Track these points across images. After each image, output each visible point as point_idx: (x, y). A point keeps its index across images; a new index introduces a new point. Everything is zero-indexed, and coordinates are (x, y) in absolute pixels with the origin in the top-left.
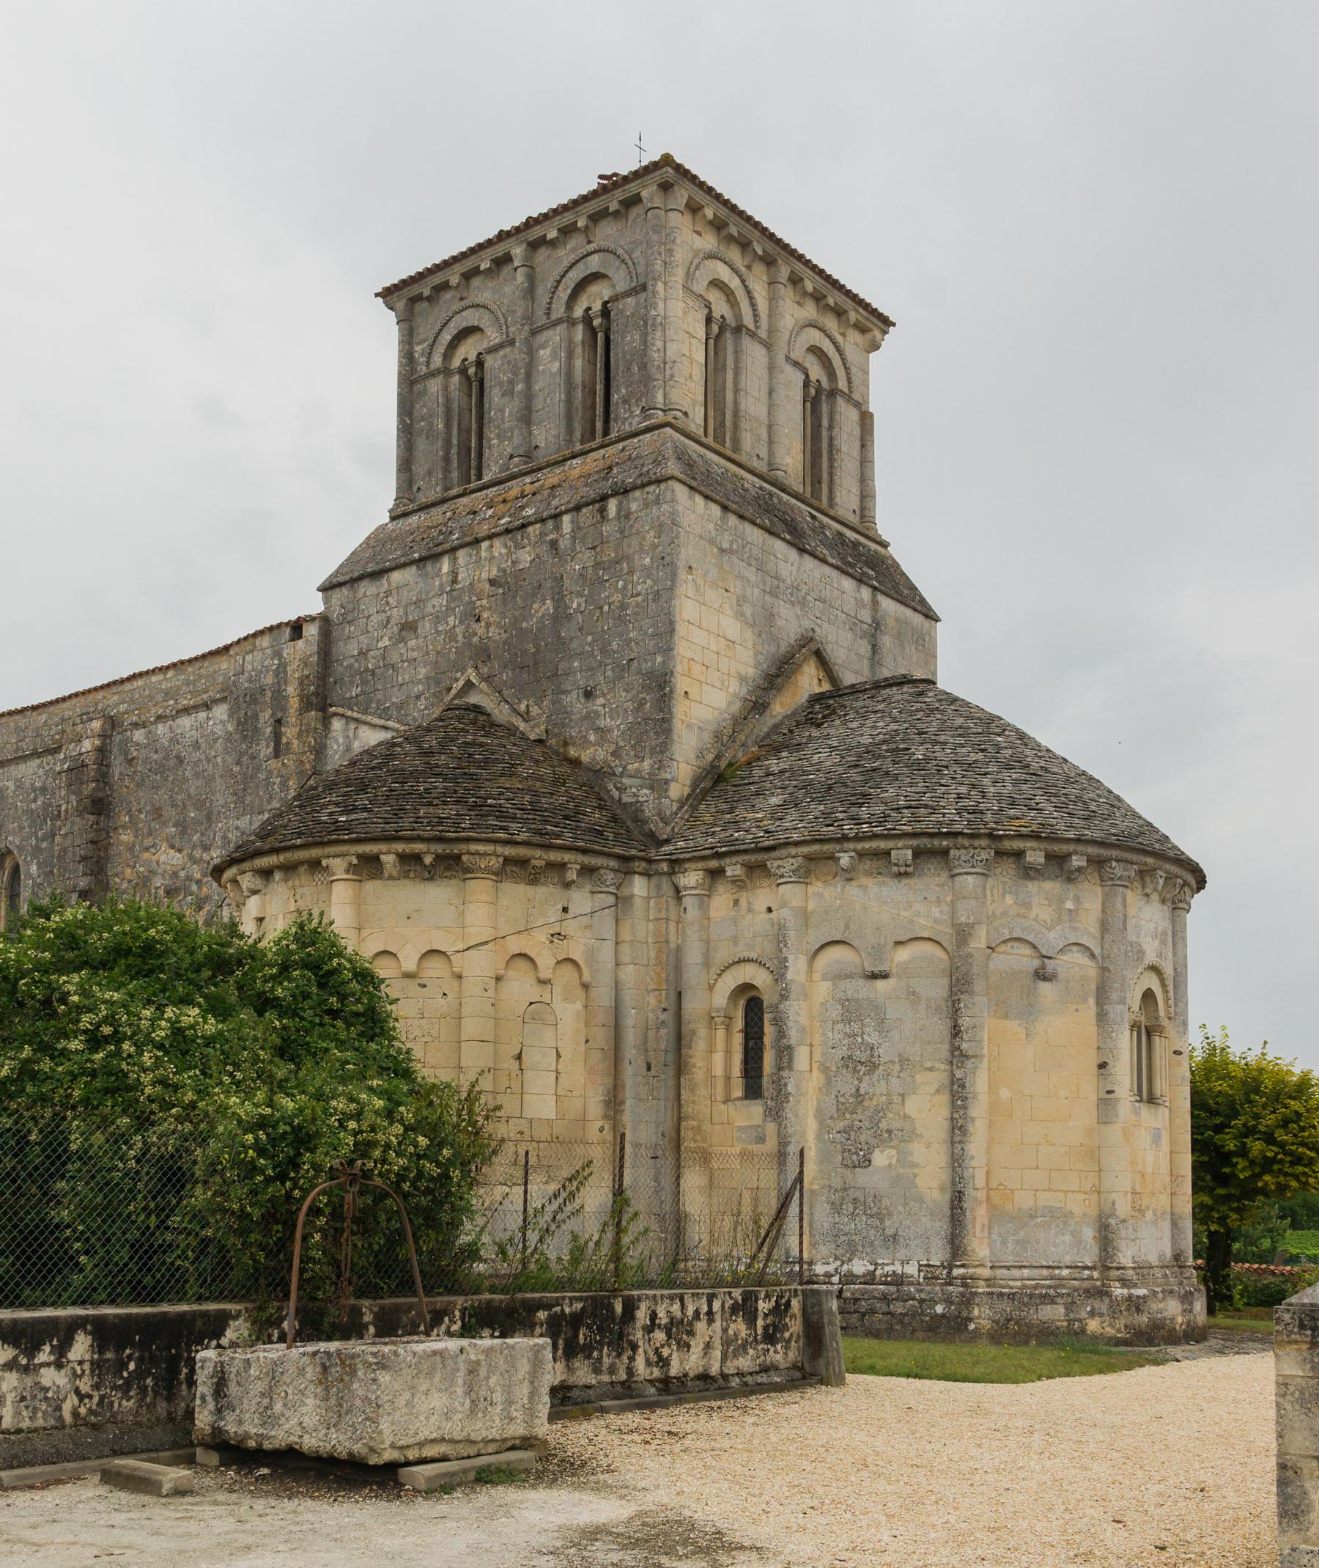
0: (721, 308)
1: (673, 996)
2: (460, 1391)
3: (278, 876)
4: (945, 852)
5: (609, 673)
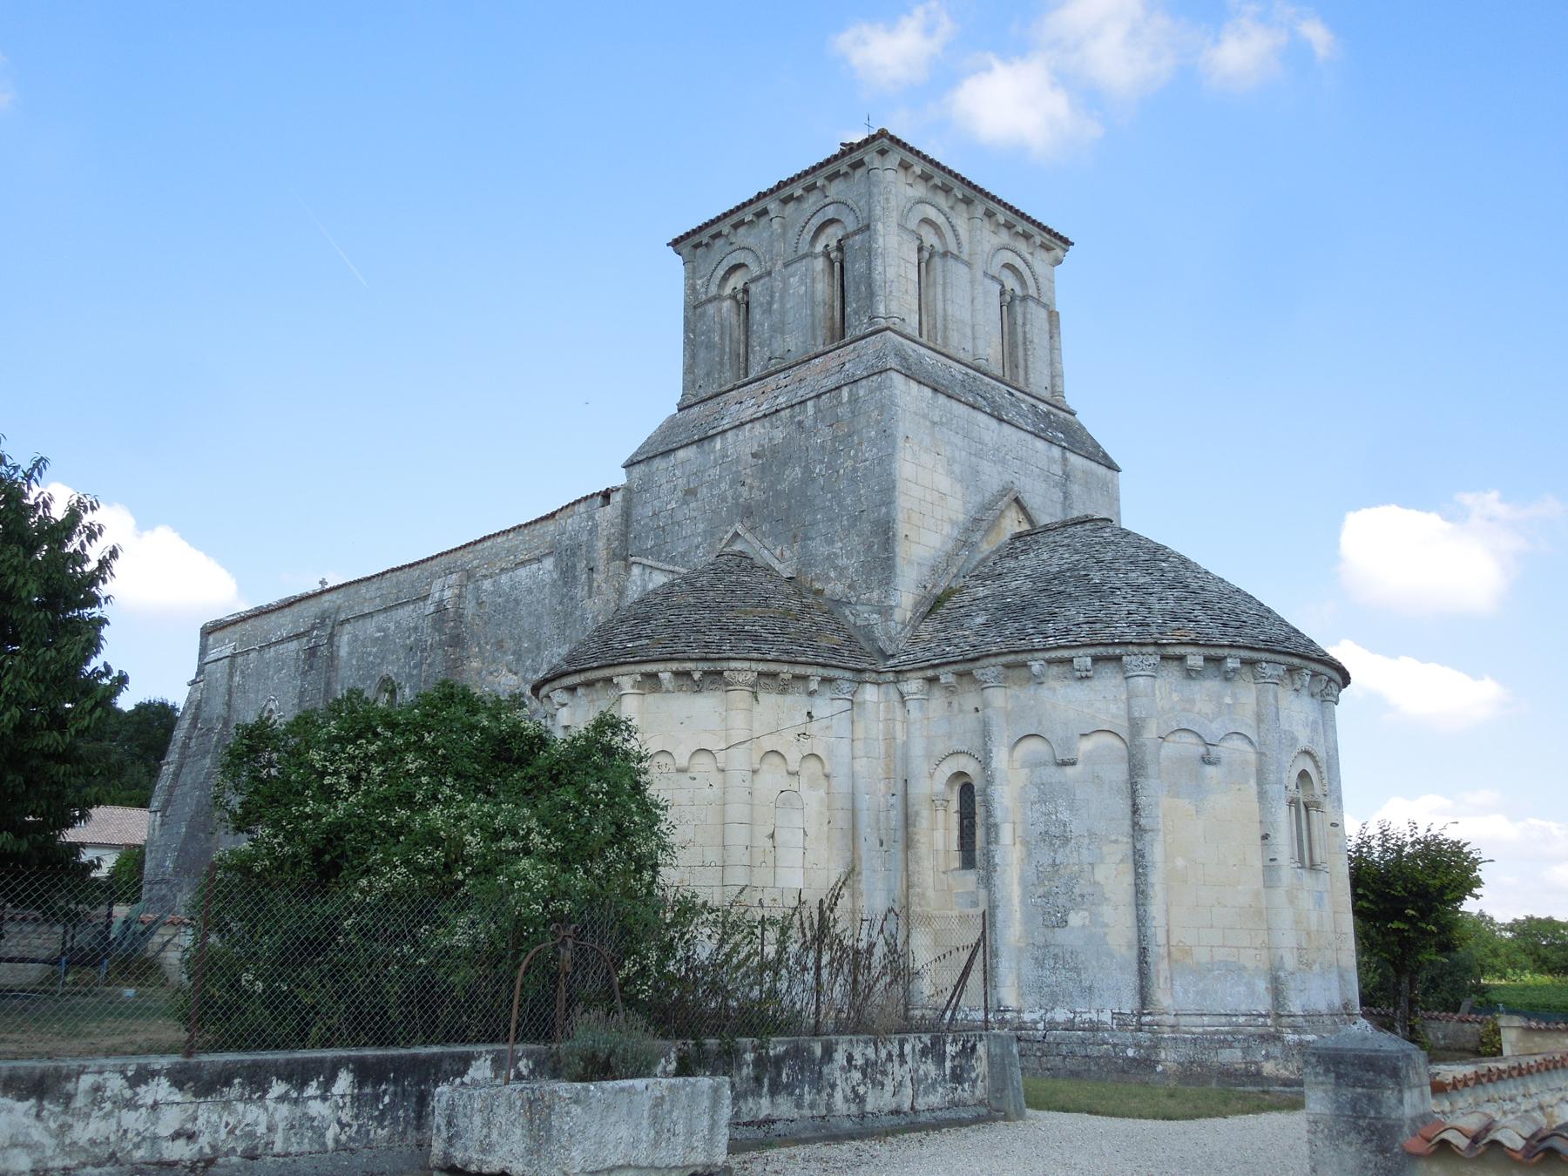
0: (930, 238)
1: (900, 784)
2: (645, 1123)
3: (580, 691)
4: (1119, 658)
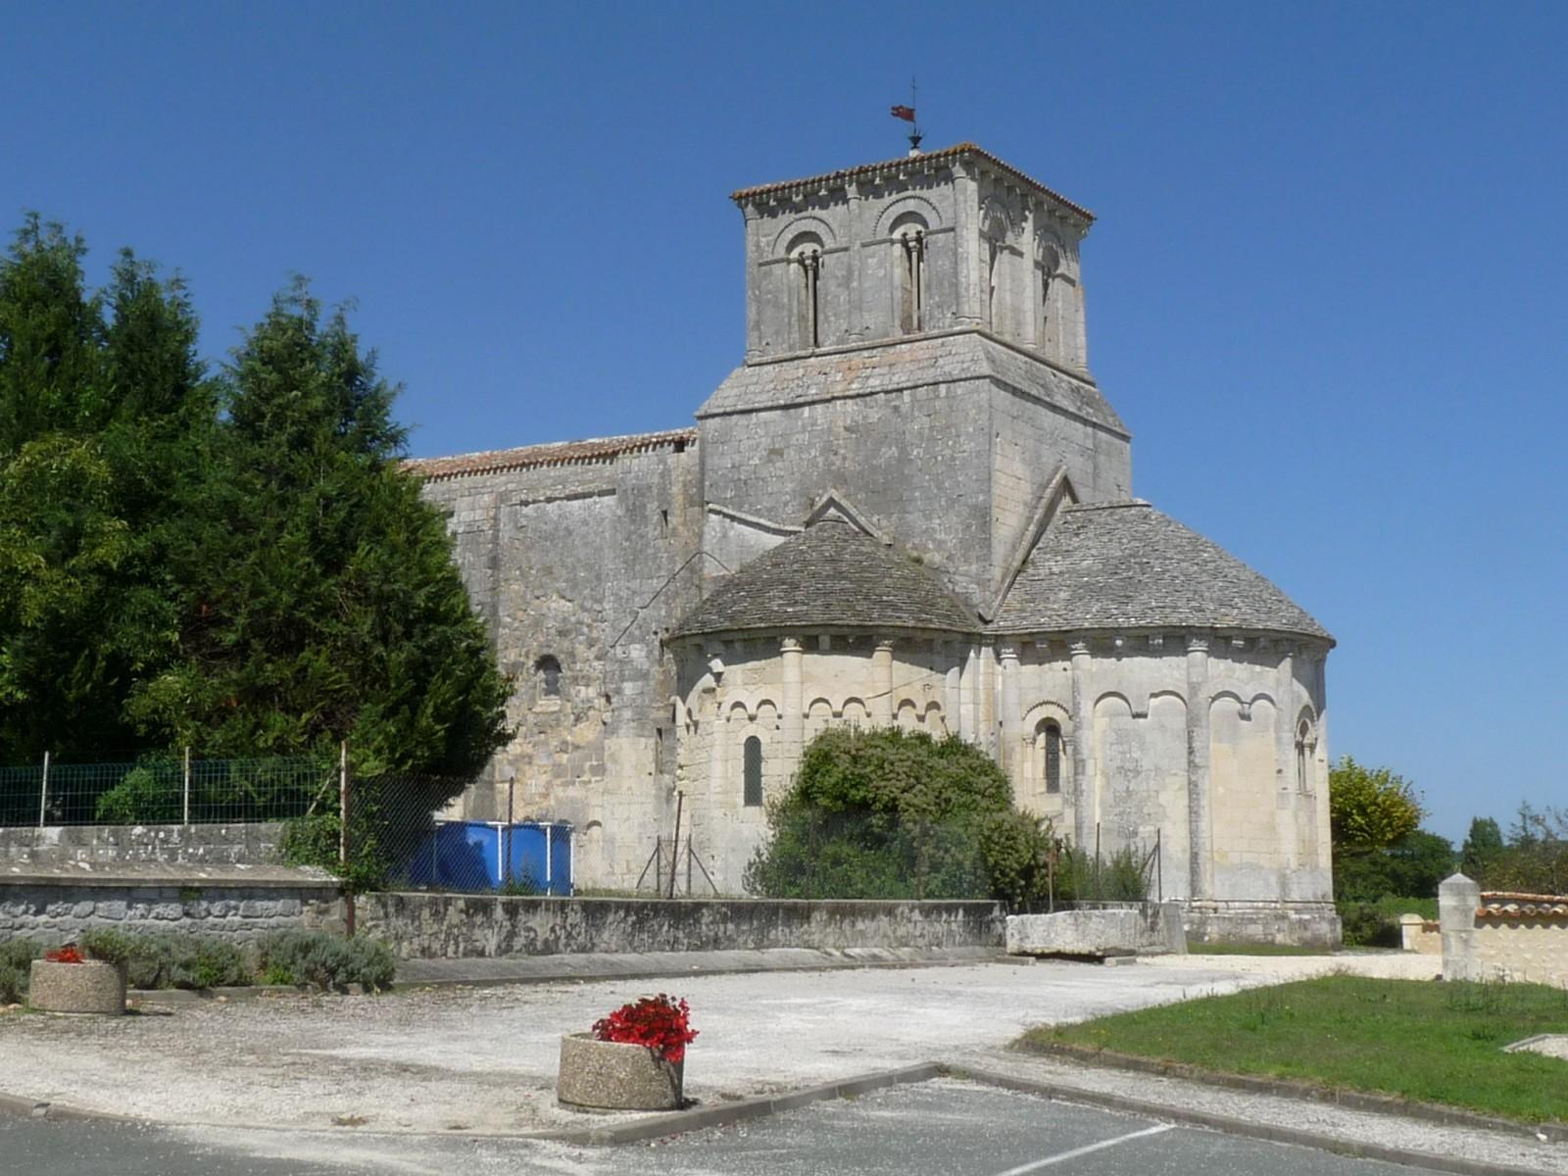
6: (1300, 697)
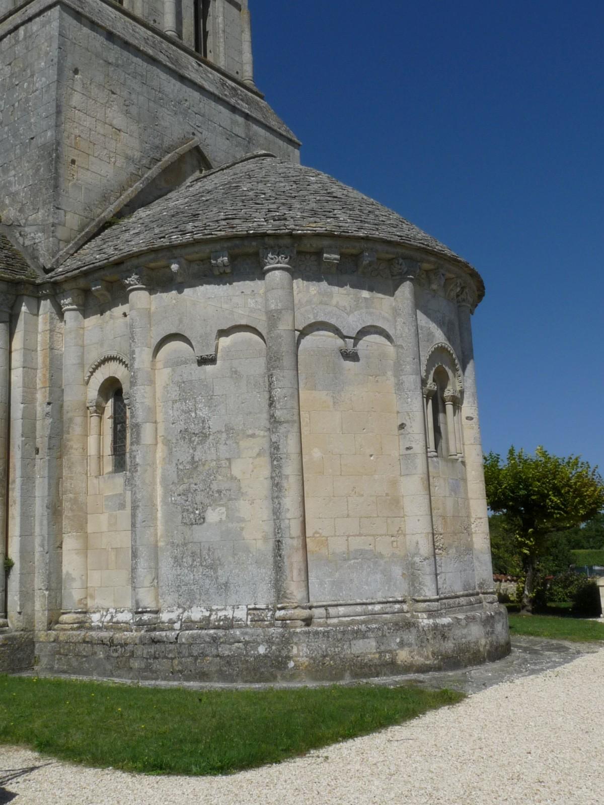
5: (18, 151)
6: (430, 335)
